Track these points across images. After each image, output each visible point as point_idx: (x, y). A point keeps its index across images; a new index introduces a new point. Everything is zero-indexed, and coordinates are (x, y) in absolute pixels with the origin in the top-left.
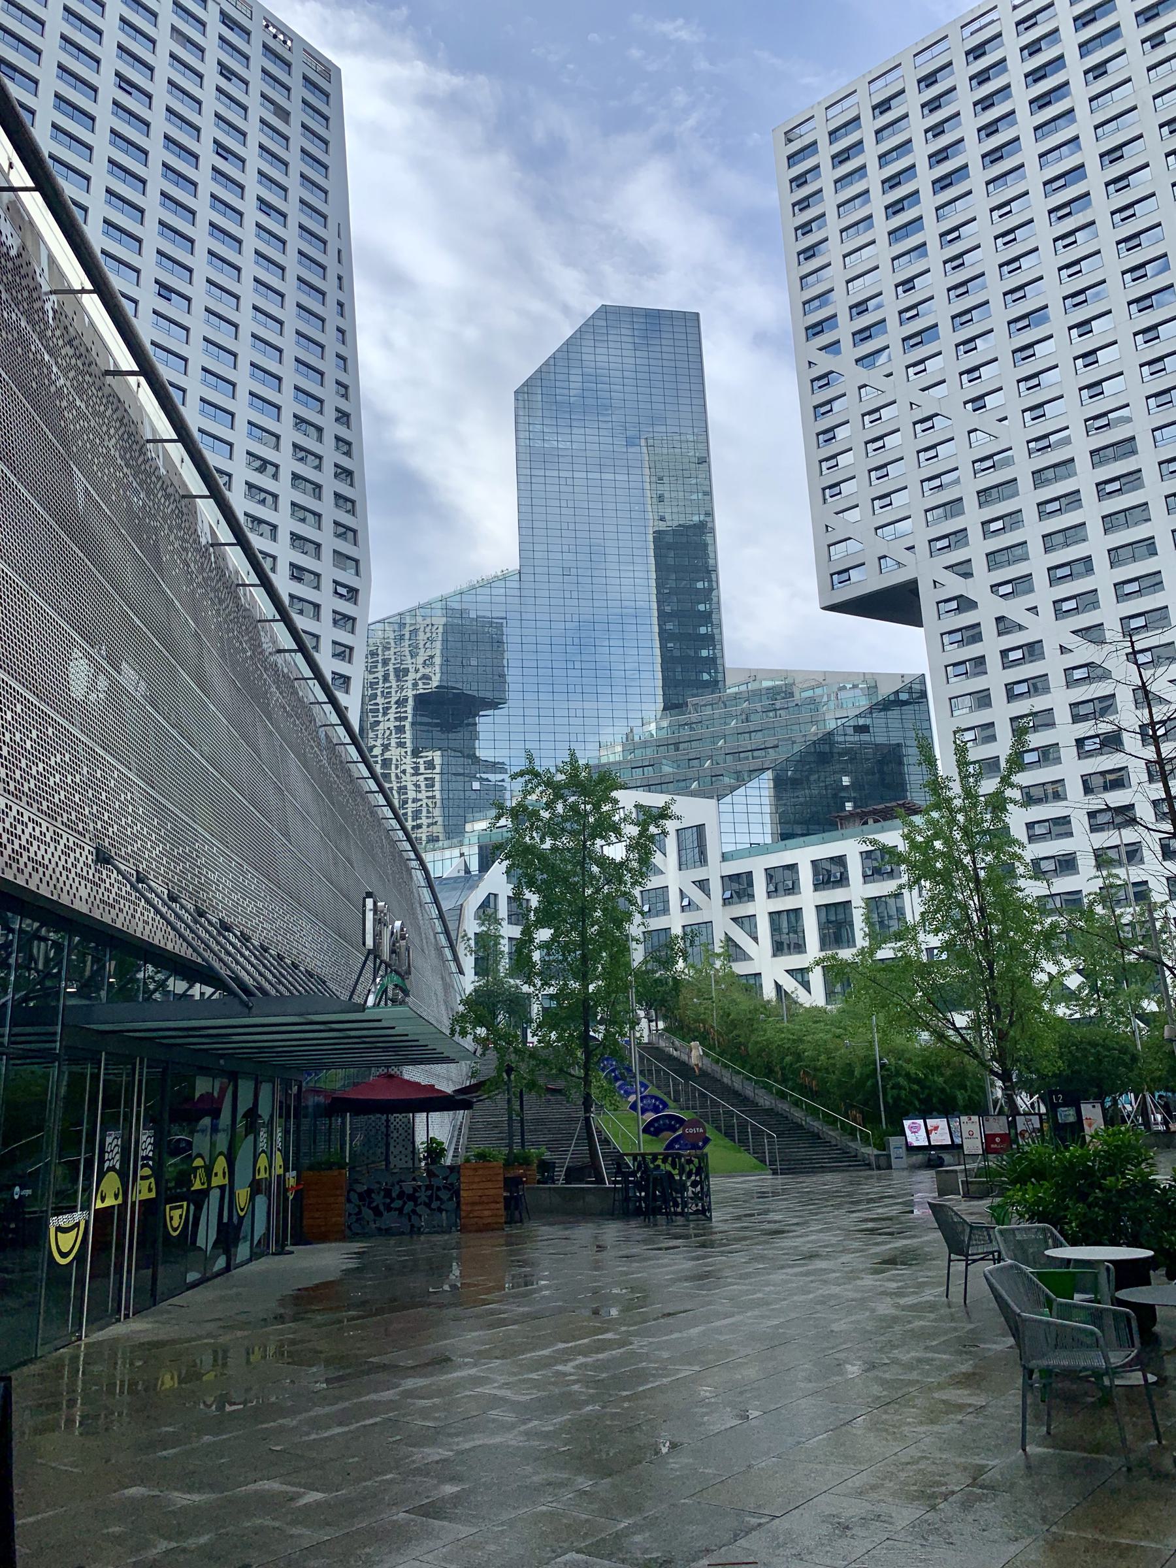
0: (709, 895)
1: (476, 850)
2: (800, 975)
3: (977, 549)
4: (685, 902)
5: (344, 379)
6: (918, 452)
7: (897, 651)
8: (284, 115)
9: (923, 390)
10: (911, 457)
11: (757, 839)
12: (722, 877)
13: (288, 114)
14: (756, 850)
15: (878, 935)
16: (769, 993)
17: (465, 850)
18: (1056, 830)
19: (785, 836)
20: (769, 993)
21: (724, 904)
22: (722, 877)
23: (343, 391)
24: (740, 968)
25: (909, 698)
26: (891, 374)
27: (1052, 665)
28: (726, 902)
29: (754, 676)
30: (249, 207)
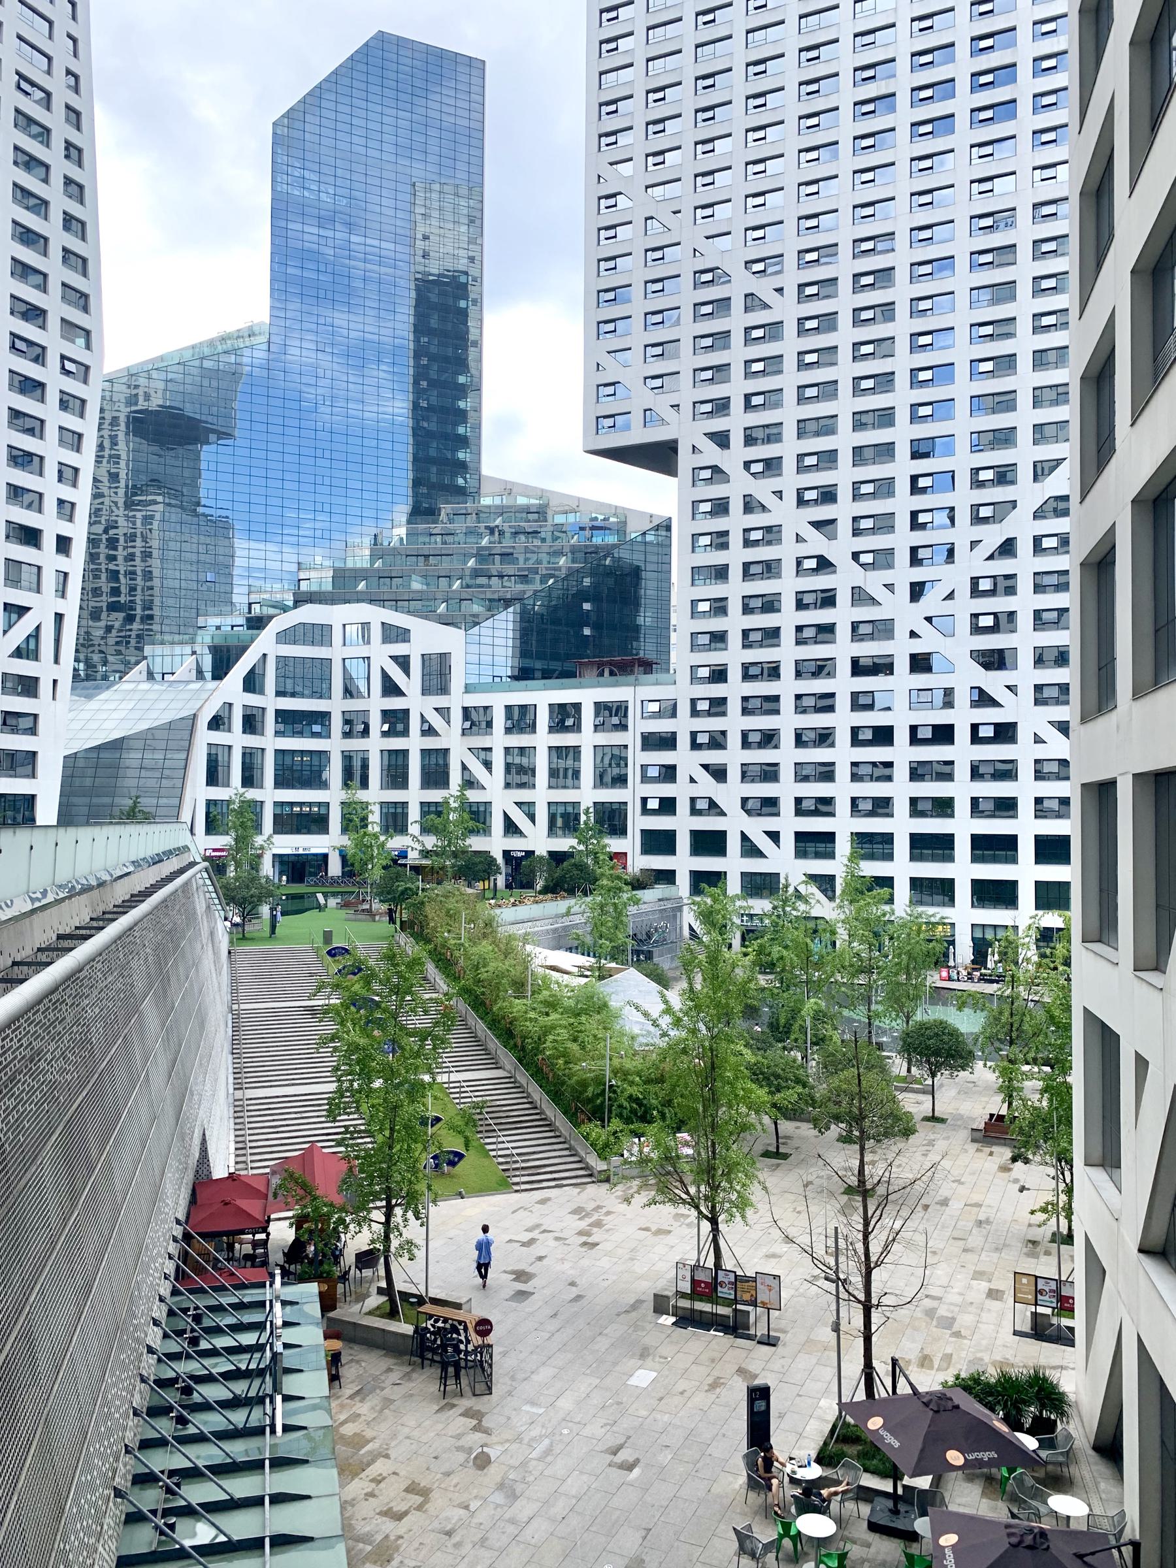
0: (448, 723)
4: (426, 727)
5: (75, 102)
6: (696, 176)
7: (647, 495)
10: (688, 115)
17: (198, 649)
18: (767, 706)
21: (463, 734)
24: (473, 796)
27: (786, 552)
28: (464, 732)
29: (509, 489)
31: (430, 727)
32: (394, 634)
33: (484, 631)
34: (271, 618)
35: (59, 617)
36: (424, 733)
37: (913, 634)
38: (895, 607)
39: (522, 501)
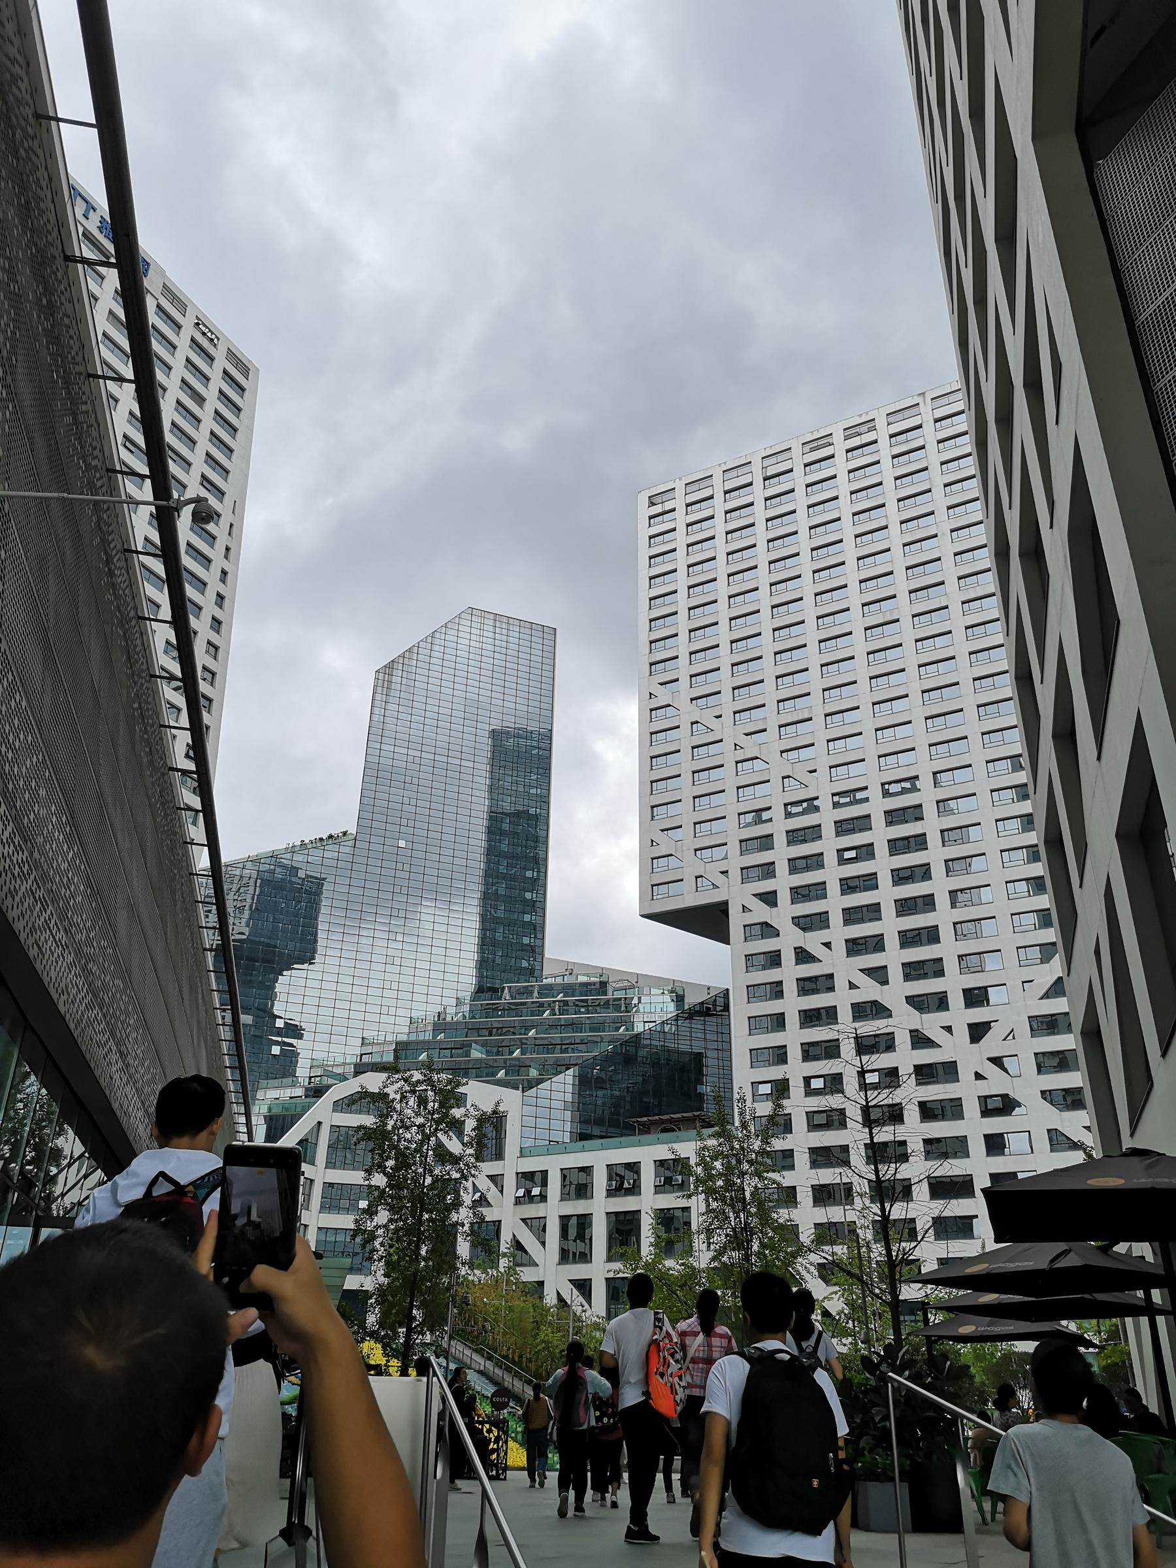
2: (584, 1287)
3: (783, 882)
7: (704, 964)
8: (200, 400)
9: (747, 735)
12: (517, 1174)
13: (204, 400)
14: (553, 1147)
15: (666, 1247)
16: (550, 1299)
19: (583, 1137)
20: (550, 1299)
22: (517, 1174)
23: (212, 650)
24: (528, 1275)
25: (714, 1009)
33: (541, 1093)
34: (329, 1087)
37: (978, 1076)
38: (954, 1048)
39: (582, 979)
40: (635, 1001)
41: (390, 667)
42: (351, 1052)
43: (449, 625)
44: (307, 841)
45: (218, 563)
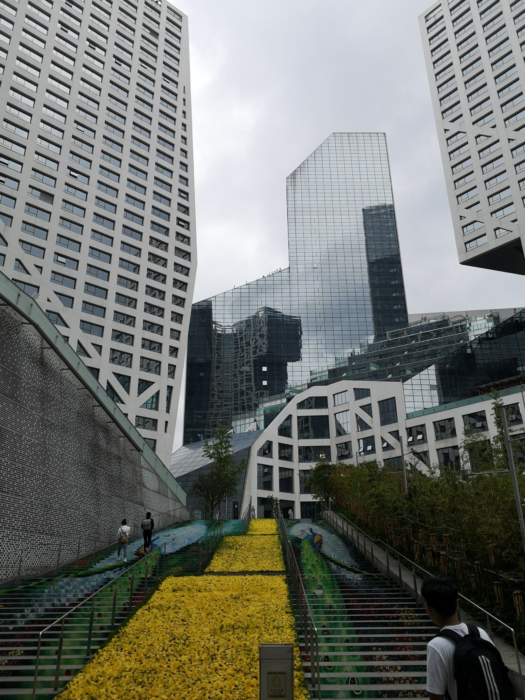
1: (262, 417)
4: (385, 445)
8: (155, 34)
11: (428, 405)
17: (257, 419)
26: (516, 220)
30: (155, 115)
31: (388, 445)
32: (361, 393)
34: (293, 397)
35: (170, 388)
36: (384, 449)
40: (468, 326)
41: (293, 175)
42: (306, 378)
43: (323, 145)
44: (266, 276)
45: (180, 119)
